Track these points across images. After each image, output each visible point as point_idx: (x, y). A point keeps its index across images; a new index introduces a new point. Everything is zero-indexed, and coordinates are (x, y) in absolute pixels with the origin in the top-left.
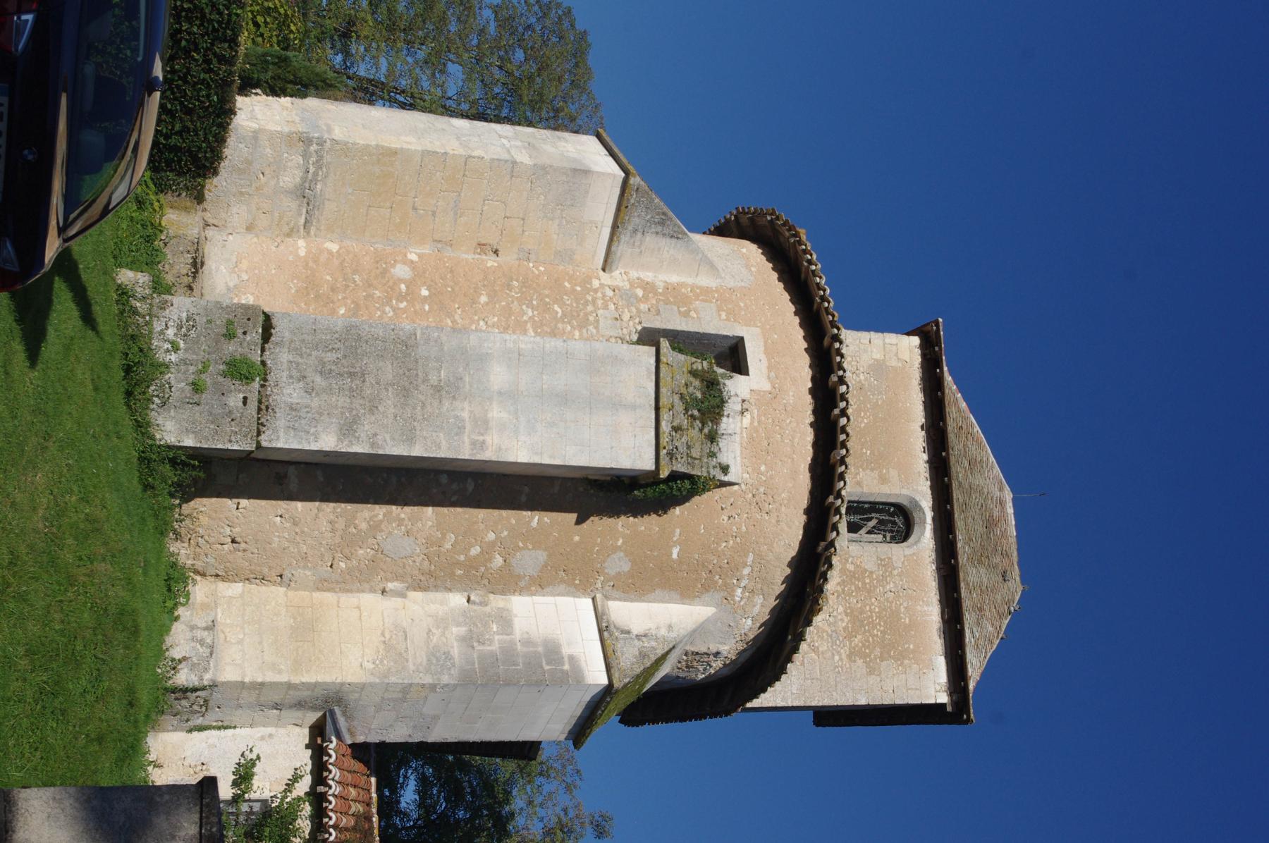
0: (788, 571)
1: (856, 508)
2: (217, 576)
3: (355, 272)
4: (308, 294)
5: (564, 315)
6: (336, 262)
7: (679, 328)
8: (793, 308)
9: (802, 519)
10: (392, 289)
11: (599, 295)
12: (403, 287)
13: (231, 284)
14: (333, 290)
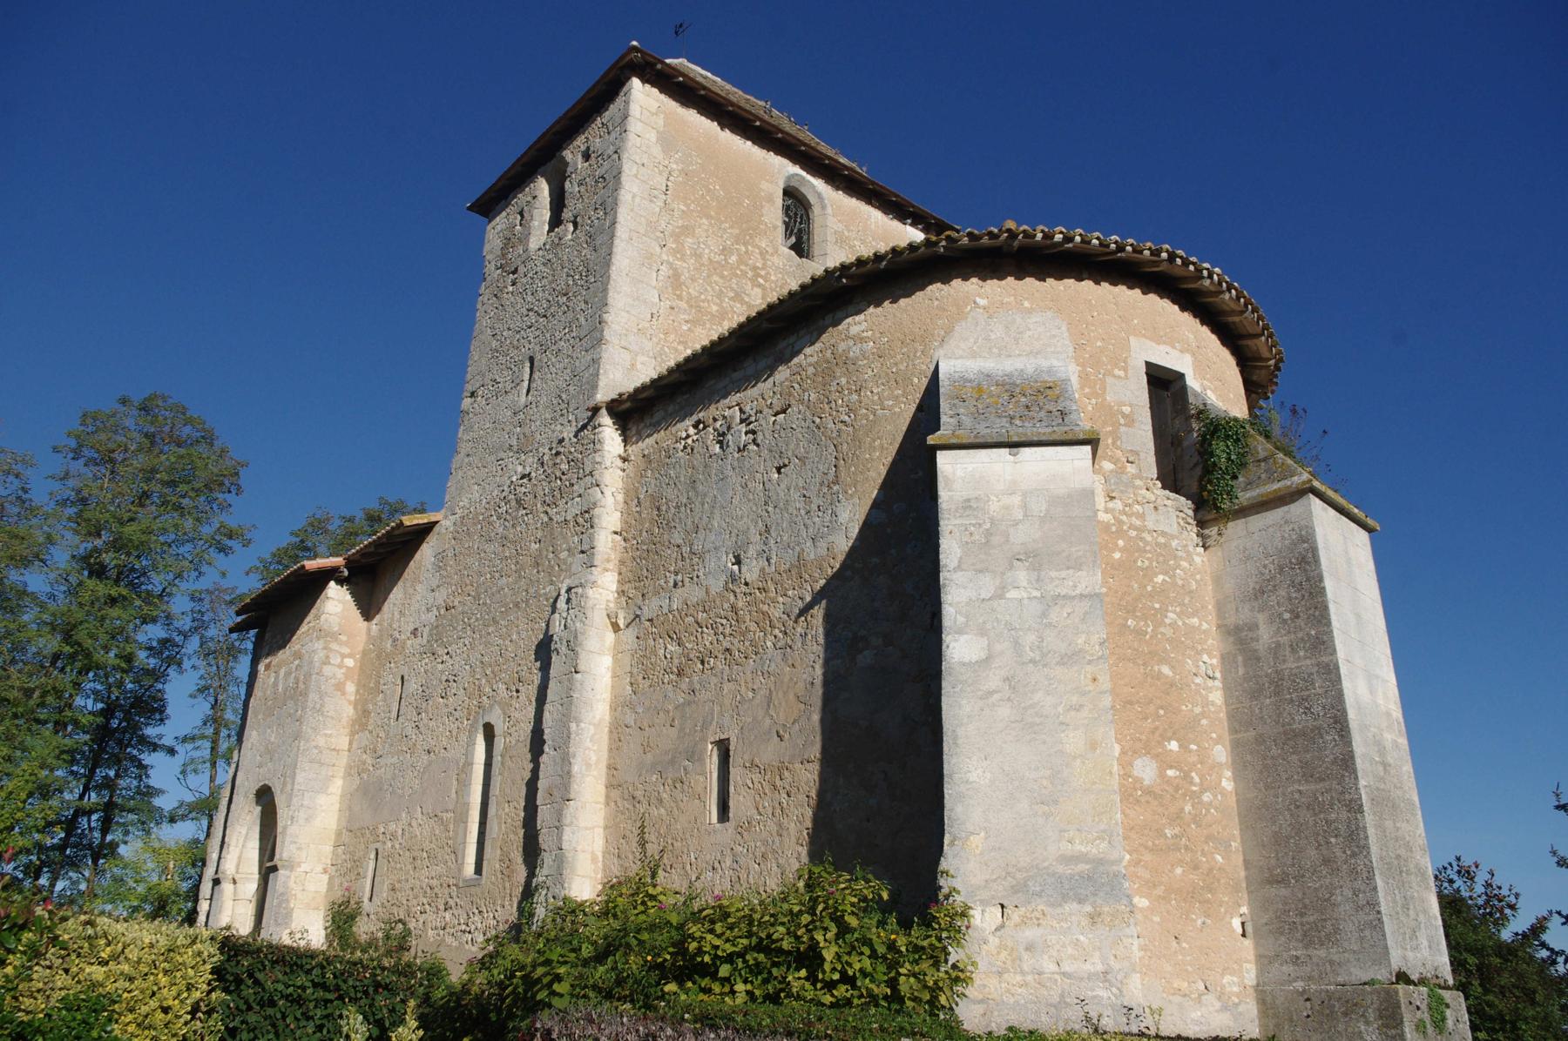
0: (886, 303)
1: (801, 248)
2: (544, 651)
3: (1160, 833)
4: (1208, 901)
5: (1166, 573)
6: (1147, 857)
7: (1149, 427)
8: (1137, 291)
9: (1153, 297)
10: (1177, 788)
11: (1124, 518)
12: (1170, 773)
13: (1218, 1005)
14: (1196, 868)
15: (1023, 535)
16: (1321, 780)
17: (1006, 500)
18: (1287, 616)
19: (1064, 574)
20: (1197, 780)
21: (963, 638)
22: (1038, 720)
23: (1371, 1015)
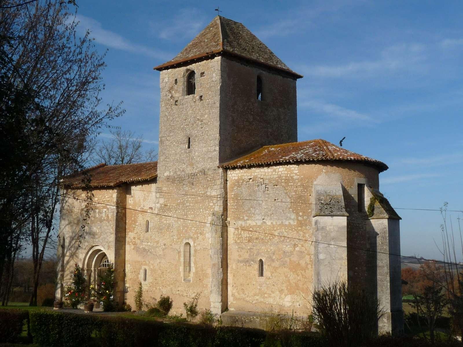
11: (351, 221)
12: (356, 274)
15: (333, 235)
16: (383, 276)
17: (330, 227)
18: (380, 243)
19: (340, 242)
20: (361, 275)
21: (321, 254)
22: (334, 270)
23: (386, 317)
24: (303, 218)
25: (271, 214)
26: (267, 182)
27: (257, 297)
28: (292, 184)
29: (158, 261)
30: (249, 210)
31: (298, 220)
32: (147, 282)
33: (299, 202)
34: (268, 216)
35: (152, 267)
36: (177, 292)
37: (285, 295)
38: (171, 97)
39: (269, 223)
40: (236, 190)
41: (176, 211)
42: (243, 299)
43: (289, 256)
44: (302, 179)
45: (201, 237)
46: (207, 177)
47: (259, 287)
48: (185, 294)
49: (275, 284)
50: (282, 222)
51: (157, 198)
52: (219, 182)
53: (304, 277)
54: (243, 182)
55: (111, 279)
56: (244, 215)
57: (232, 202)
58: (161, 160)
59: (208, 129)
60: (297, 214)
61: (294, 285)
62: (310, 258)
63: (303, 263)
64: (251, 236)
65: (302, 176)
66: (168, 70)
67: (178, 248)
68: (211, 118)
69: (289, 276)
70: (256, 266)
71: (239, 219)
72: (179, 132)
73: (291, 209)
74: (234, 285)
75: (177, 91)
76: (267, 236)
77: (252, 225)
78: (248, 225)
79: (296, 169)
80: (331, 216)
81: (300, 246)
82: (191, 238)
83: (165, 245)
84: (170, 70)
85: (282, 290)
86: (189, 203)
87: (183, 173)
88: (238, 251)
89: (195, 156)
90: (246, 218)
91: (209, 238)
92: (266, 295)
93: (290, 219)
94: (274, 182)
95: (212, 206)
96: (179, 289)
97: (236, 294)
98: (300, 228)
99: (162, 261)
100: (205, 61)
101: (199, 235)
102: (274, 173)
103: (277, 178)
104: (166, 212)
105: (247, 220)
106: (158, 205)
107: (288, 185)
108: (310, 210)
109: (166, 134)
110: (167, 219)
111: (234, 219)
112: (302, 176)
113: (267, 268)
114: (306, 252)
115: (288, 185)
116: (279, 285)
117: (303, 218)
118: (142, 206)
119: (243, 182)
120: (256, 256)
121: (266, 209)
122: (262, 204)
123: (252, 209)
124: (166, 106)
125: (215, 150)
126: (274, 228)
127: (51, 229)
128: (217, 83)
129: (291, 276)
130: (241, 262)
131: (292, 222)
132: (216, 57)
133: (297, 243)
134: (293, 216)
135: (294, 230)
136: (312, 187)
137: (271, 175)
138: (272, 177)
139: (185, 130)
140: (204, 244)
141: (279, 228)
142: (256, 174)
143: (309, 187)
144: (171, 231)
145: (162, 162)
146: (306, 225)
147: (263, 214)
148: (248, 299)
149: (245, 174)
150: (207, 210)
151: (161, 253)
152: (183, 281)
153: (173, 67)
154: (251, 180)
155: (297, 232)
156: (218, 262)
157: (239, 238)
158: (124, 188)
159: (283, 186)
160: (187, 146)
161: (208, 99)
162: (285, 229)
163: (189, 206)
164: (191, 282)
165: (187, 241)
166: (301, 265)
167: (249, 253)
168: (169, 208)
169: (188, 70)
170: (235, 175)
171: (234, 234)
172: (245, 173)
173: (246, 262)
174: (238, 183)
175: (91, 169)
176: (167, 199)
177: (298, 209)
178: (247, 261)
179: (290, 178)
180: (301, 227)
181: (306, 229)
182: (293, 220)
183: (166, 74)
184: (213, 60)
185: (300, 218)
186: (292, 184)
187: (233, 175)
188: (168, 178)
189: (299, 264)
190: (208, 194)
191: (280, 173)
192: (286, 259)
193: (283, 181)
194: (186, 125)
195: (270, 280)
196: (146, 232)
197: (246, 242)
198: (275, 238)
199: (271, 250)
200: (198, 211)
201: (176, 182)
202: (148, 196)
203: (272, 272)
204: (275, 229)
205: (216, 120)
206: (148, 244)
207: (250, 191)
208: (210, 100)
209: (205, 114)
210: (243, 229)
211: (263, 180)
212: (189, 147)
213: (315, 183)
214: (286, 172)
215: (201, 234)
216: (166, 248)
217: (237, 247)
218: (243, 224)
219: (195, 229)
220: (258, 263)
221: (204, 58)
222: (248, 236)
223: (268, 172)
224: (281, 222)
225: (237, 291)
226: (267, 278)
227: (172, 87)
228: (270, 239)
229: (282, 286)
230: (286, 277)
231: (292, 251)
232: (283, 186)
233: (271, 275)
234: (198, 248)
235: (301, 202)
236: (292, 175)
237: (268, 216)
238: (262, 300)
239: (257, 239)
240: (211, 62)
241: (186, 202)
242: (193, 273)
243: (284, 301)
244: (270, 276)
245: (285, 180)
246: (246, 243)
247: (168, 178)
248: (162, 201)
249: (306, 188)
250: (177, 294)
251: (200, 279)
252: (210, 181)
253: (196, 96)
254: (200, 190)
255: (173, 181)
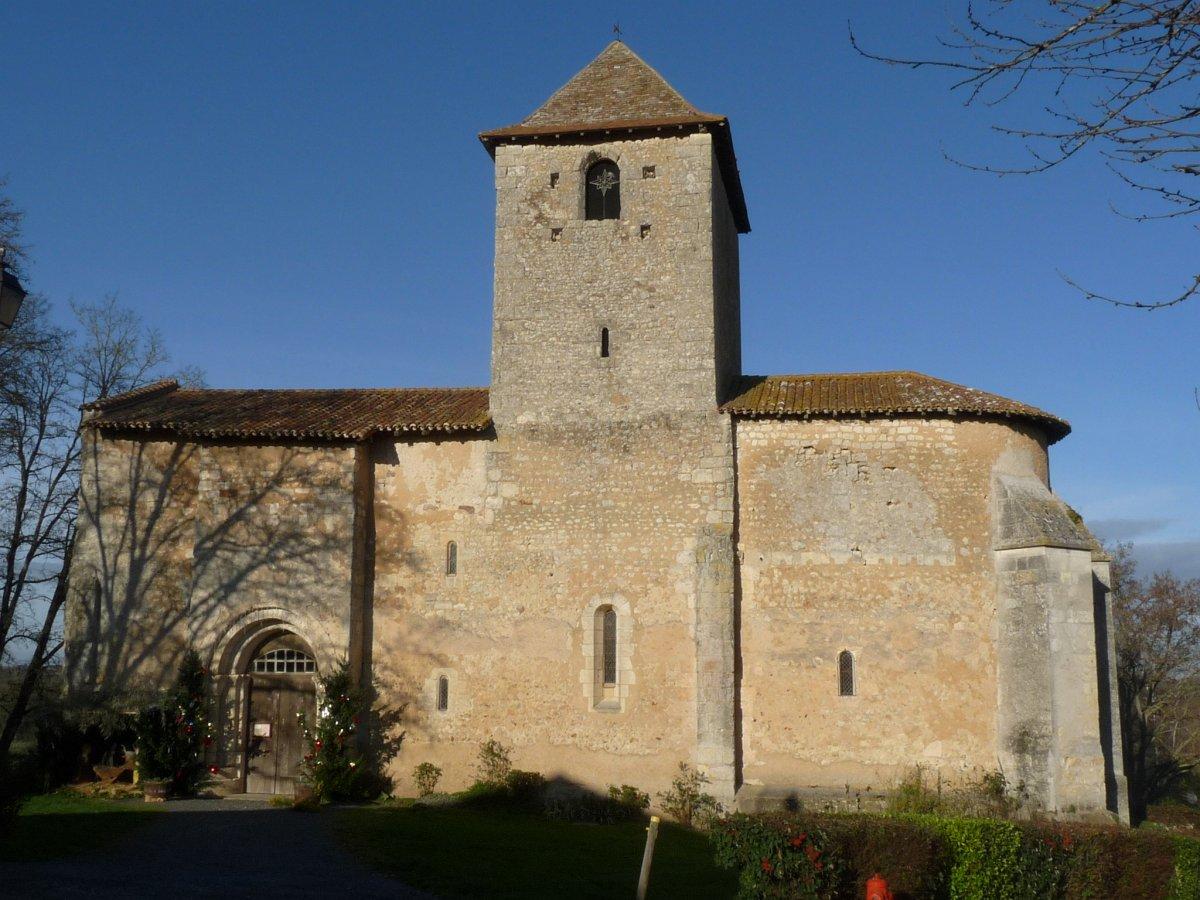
24: (971, 550)
25: (878, 539)
26: (862, 457)
27: (834, 749)
28: (940, 467)
29: (496, 654)
30: (808, 524)
31: (959, 555)
32: (449, 713)
33: (959, 514)
34: (869, 542)
35: (469, 670)
36: (570, 741)
37: (926, 742)
38: (536, 218)
39: (872, 559)
40: (762, 475)
41: (567, 517)
42: (790, 753)
43: (936, 644)
44: (963, 459)
45: (656, 592)
46: (677, 436)
47: (841, 723)
48: (597, 744)
49: (892, 714)
50: (914, 559)
51: (490, 481)
52: (722, 449)
53: (977, 695)
54: (786, 454)
55: (360, 712)
56: (792, 539)
57: (749, 502)
58: (505, 380)
59: (673, 312)
60: (957, 540)
61: (951, 715)
62: (992, 649)
63: (973, 661)
64: (813, 590)
65: (965, 451)
66: (525, 147)
67: (572, 620)
68: (684, 286)
69: (936, 693)
70: (834, 669)
71: (776, 547)
72: (571, 311)
73: (940, 529)
74: (760, 719)
75: (559, 203)
76: (866, 594)
77: (819, 563)
78: (805, 564)
79: (950, 431)
80: (1067, 548)
81: (964, 618)
82: (623, 592)
83: (522, 610)
84: (531, 148)
85: (916, 728)
86: (615, 500)
87: (590, 420)
88: (772, 629)
89: (630, 378)
90: (796, 545)
91: (686, 596)
92: (863, 743)
93: (939, 552)
94: (885, 458)
95: (697, 510)
96: (576, 730)
97: (766, 742)
98: (963, 576)
99: (512, 655)
100: (657, 139)
101: (650, 585)
102: (883, 437)
103: (893, 449)
104: (528, 522)
105: (801, 550)
106: (497, 502)
107: (928, 470)
108: (986, 534)
109: (520, 312)
110: (529, 539)
111: (757, 546)
112: (965, 451)
113: (865, 672)
114: (981, 635)
115: (928, 470)
116: (907, 718)
117: (971, 550)
118: (432, 501)
119: (786, 454)
120: (831, 642)
121: (861, 524)
122: (848, 512)
123: (816, 523)
124: (519, 239)
125: (701, 368)
126: (886, 572)
127: (1048, 496)
128: (701, 199)
129: (943, 694)
130: (782, 657)
131: (943, 561)
132: (698, 132)
133: (957, 612)
134: (947, 545)
135: (948, 579)
136: (989, 477)
137: (874, 442)
138: (877, 446)
139: (593, 306)
140: (670, 609)
141: (902, 573)
142: (826, 436)
143: (983, 477)
144: (548, 572)
145: (509, 384)
146: (979, 569)
147: (852, 537)
148: (806, 754)
149: (792, 435)
150: (679, 521)
151: (509, 631)
152: (590, 709)
153: (547, 139)
154: (810, 451)
155: (959, 585)
156: (724, 657)
157: (772, 597)
158: (378, 447)
159: (913, 472)
160: (599, 350)
161: (673, 237)
162: (922, 577)
163: (615, 507)
164: (623, 711)
165: (607, 601)
166: (969, 667)
167: (807, 636)
168: (539, 510)
169: (593, 155)
170: (760, 435)
171: (757, 586)
172: (791, 431)
173: (798, 657)
174: (771, 456)
175: (137, 396)
176: (532, 485)
177: (959, 530)
178: (803, 656)
179: (934, 453)
180: (968, 573)
181: (980, 579)
182: (948, 554)
183: (518, 156)
184: (685, 139)
185: (964, 552)
186: (940, 467)
187: (752, 435)
188: (533, 431)
189: (963, 665)
190: (682, 477)
191: (902, 439)
192: (928, 651)
193: (912, 458)
194: (593, 295)
195: (875, 705)
196: (447, 574)
197: (800, 608)
198: (892, 598)
199: (879, 628)
200: (647, 523)
201: (565, 441)
202: (455, 476)
203: (882, 684)
204: (892, 576)
205: (704, 291)
206: (455, 606)
207: (809, 478)
208: (676, 238)
209: (664, 272)
210: (785, 569)
211: (852, 452)
212: (605, 353)
213: (995, 468)
214: (921, 438)
215: (656, 582)
216: (526, 620)
217: (768, 619)
218: (789, 560)
219: (637, 569)
220: (837, 659)
221: (630, 131)
222: (803, 590)
223: (866, 435)
224: (910, 559)
225: (768, 733)
226: (866, 699)
227: (541, 192)
228: (874, 599)
229: (915, 719)
230: (929, 694)
231: (945, 630)
232: (913, 472)
233: (881, 690)
234: (647, 620)
235: (964, 511)
236: (937, 445)
237: (869, 542)
238: (852, 755)
239: (833, 598)
240: (676, 144)
241: (600, 496)
242: (630, 686)
243: (923, 756)
244: (876, 693)
245: (920, 455)
246: (798, 611)
247: (532, 431)
248: (510, 490)
249: (976, 478)
250: (568, 746)
251: (653, 704)
252: (690, 445)
253: (629, 225)
254: (653, 467)
255: (555, 437)
